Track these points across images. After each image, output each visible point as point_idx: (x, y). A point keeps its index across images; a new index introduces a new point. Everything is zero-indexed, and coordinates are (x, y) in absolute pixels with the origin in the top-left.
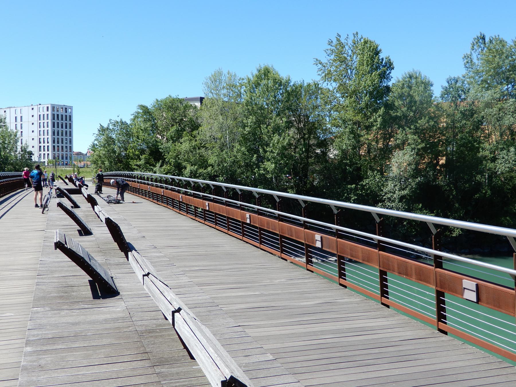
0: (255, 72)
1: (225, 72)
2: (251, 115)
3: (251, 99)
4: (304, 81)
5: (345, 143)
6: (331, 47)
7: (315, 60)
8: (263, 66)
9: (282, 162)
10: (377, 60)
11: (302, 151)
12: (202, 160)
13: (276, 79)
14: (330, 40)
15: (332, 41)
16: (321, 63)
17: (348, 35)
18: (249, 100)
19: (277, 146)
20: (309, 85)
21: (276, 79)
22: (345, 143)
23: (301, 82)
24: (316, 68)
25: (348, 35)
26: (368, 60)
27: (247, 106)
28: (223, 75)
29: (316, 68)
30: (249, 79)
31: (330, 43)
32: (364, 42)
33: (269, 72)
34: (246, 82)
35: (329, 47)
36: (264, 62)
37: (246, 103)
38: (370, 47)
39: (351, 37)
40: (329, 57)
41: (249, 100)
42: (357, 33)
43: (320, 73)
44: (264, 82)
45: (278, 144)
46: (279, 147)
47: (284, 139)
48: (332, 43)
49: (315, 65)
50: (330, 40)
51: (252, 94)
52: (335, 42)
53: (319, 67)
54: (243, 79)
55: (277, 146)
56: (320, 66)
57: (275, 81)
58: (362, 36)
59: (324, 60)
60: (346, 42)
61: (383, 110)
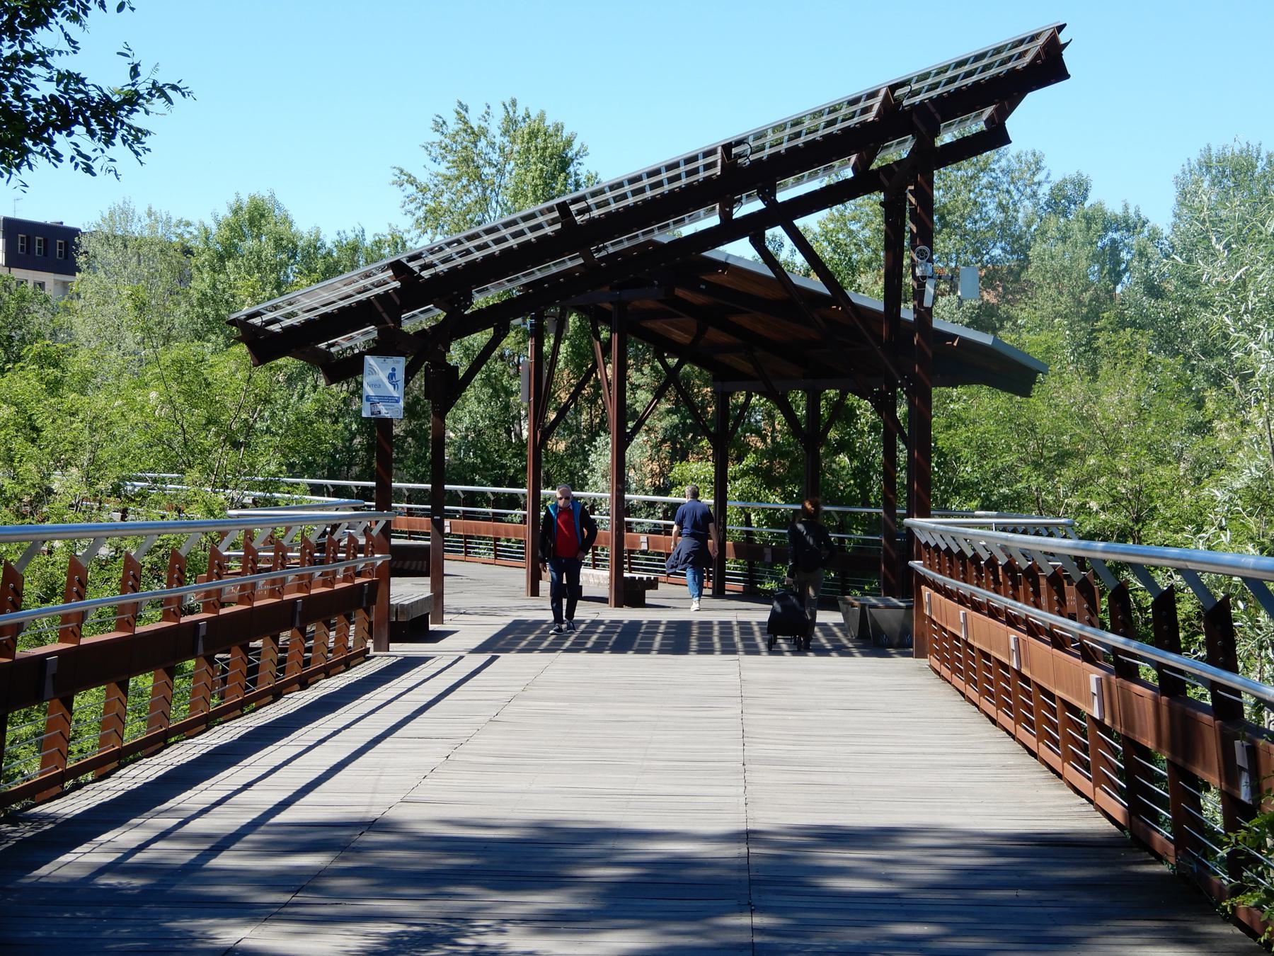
0: (225, 213)
1: (141, 210)
2: (211, 330)
3: (214, 287)
4: (363, 231)
5: (470, 412)
6: (442, 138)
7: (397, 172)
8: (246, 200)
9: (1234, 246)
10: (562, 185)
11: (350, 431)
12: (225, 476)
13: (282, 239)
14: (438, 119)
15: (444, 123)
16: (412, 181)
17: (489, 107)
18: (208, 291)
19: (282, 416)
20: (378, 244)
21: (282, 239)
22: (470, 412)
23: (357, 232)
24: (398, 195)
25: (489, 107)
26: (536, 186)
27: (201, 306)
28: (136, 220)
29: (398, 195)
30: (205, 229)
31: (440, 125)
32: (529, 133)
33: (262, 216)
34: (196, 233)
35: (437, 137)
36: (249, 188)
37: (198, 299)
38: (545, 149)
39: (498, 115)
40: (436, 164)
41: (208, 291)
42: (514, 103)
43: (412, 207)
44: (250, 244)
45: (285, 412)
46: (287, 418)
47: (301, 397)
48: (444, 127)
49: (395, 186)
50: (438, 119)
51: (216, 275)
52: (453, 125)
53: (407, 193)
54: (188, 224)
55: (282, 416)
56: (411, 189)
57: (278, 243)
58: (527, 109)
59: (423, 178)
60: (483, 124)
61: (575, 323)
